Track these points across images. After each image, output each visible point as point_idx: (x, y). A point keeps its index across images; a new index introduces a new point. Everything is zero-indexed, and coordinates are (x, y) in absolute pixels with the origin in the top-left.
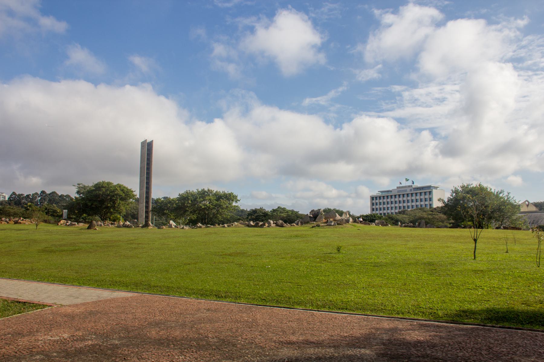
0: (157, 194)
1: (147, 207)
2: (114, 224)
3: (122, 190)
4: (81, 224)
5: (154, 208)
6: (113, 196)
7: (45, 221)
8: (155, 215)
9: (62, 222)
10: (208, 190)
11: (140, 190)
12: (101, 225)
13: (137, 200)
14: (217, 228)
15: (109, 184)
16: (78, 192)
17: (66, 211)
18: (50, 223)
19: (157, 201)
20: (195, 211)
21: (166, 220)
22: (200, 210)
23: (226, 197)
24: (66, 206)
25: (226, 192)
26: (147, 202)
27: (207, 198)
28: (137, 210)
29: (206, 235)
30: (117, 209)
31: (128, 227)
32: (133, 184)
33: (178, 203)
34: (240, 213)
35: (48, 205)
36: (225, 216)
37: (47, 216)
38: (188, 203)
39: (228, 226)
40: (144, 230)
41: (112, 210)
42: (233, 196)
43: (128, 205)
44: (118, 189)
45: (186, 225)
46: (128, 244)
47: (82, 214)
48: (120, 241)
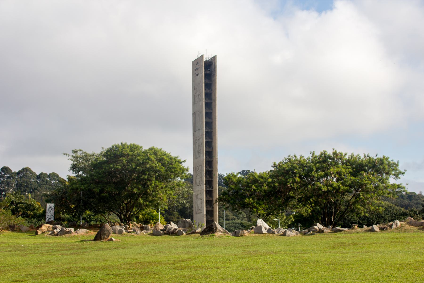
0: (227, 165)
1: (209, 193)
2: (146, 229)
3: (160, 160)
4: (82, 231)
5: (224, 194)
6: (143, 173)
7: (12, 228)
8: (226, 209)
9: (45, 227)
10: (335, 153)
11: (195, 157)
12: (120, 232)
13: (190, 179)
14: (358, 234)
15: (133, 148)
16: (74, 168)
17: (53, 205)
18: (20, 230)
19: (227, 181)
20: (307, 198)
21: (249, 220)
22: (319, 196)
23: (374, 166)
24: (51, 195)
25: (373, 156)
26: (209, 183)
27: (332, 170)
28: (190, 198)
29: (333, 247)
30: (150, 198)
31: (173, 233)
32: (181, 148)
33: (273, 182)
34: (406, 202)
35: (15, 195)
36: (372, 208)
37: (14, 217)
38: (294, 182)
39: (382, 229)
40: (207, 239)
41: (141, 201)
42: (389, 165)
43: (172, 189)
44: (152, 157)
45: (290, 227)
46: (176, 268)
47: (83, 211)
48: (159, 263)
